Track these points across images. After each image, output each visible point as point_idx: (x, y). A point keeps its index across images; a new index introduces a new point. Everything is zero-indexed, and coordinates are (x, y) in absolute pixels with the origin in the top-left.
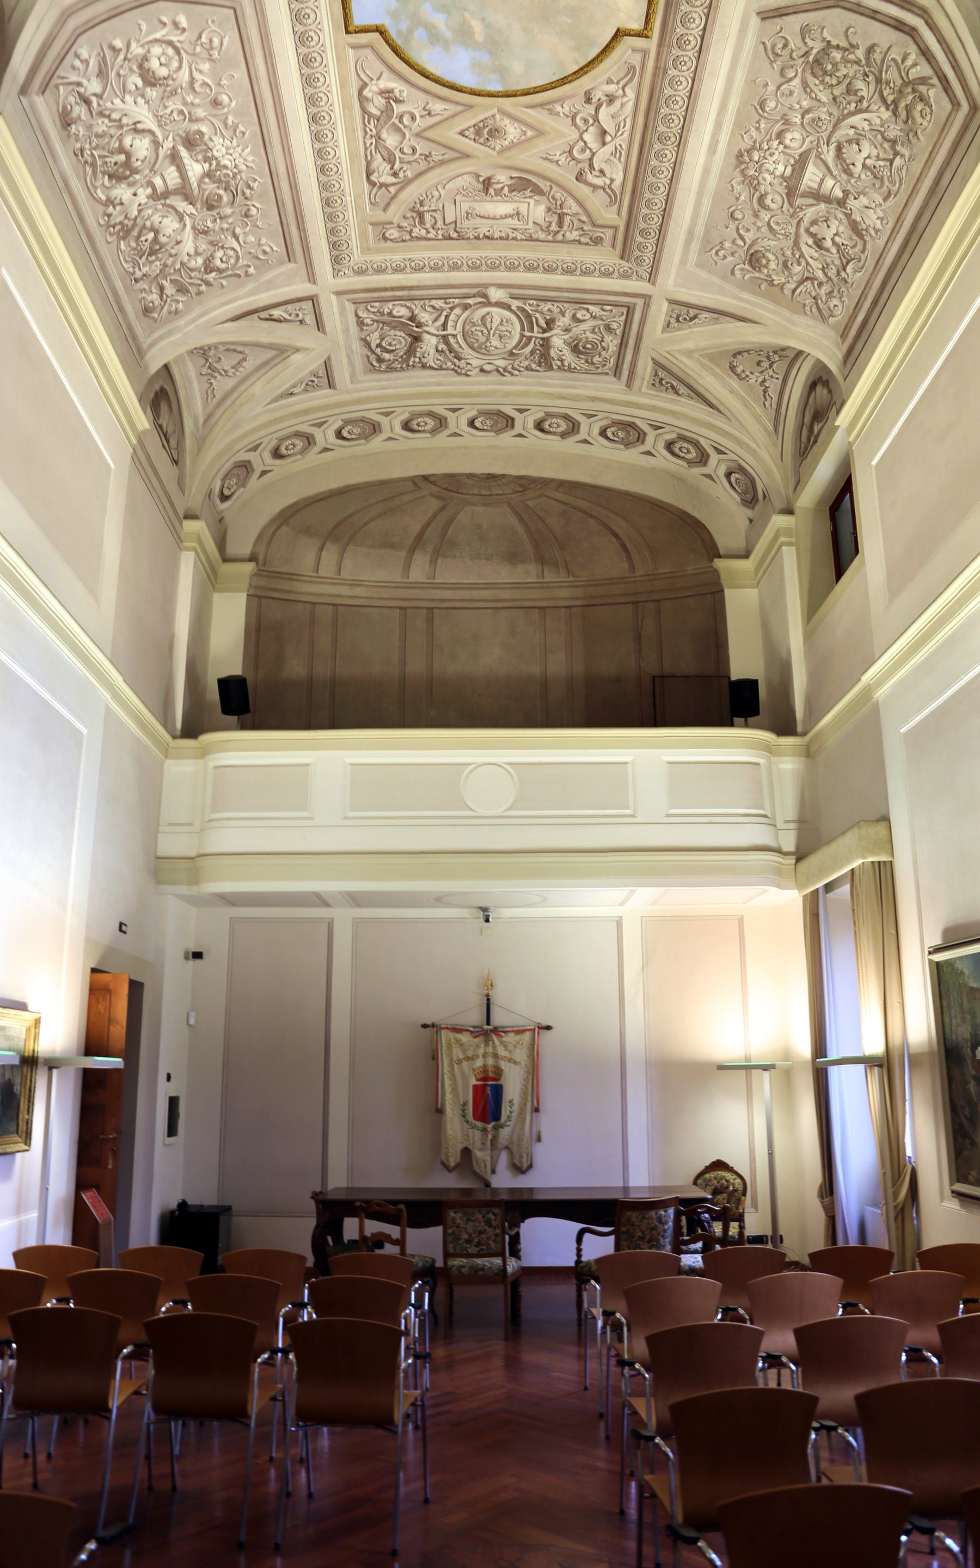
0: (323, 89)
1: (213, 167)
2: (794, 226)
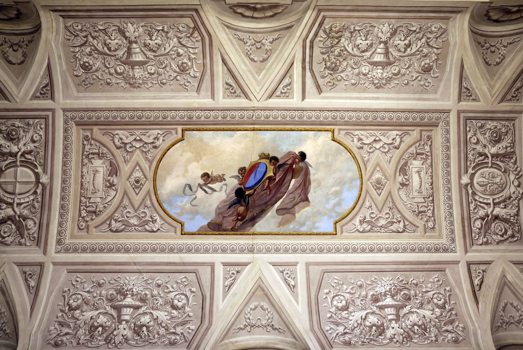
0: (176, 246)
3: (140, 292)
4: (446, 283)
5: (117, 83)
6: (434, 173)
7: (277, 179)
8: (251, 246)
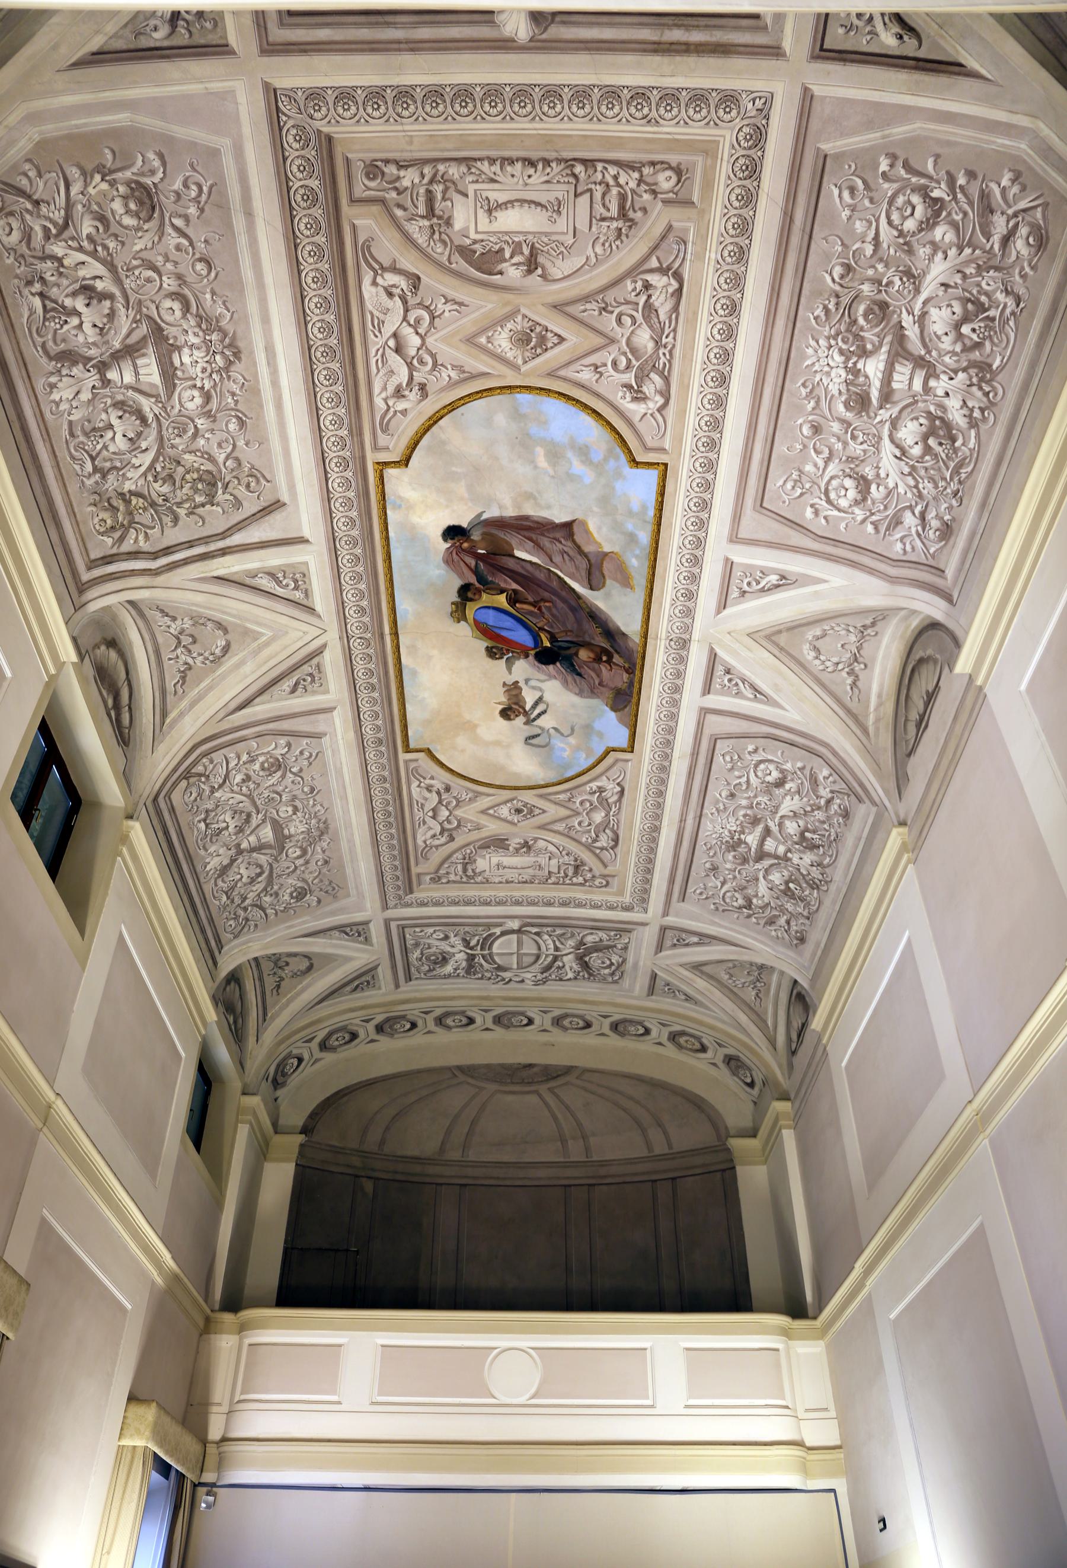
1: (855, 359)
2: (129, 291)
3: (738, 823)
4: (864, 161)
5: (324, 852)
6: (493, 154)
7: (515, 586)
8: (672, 643)
